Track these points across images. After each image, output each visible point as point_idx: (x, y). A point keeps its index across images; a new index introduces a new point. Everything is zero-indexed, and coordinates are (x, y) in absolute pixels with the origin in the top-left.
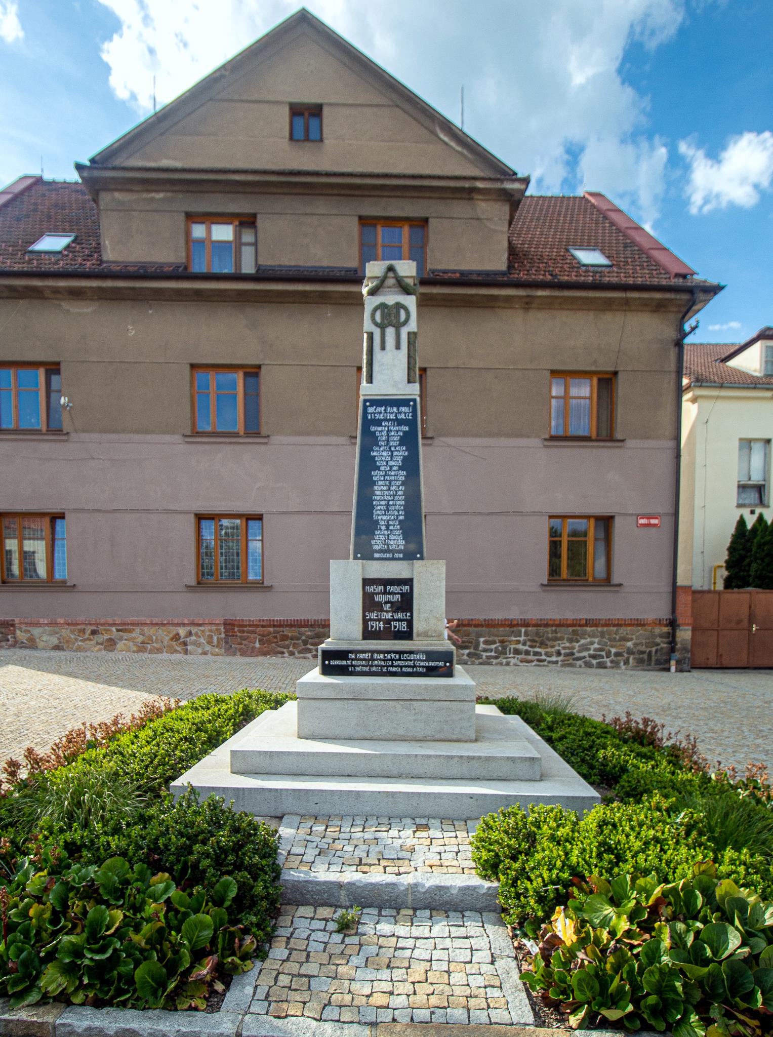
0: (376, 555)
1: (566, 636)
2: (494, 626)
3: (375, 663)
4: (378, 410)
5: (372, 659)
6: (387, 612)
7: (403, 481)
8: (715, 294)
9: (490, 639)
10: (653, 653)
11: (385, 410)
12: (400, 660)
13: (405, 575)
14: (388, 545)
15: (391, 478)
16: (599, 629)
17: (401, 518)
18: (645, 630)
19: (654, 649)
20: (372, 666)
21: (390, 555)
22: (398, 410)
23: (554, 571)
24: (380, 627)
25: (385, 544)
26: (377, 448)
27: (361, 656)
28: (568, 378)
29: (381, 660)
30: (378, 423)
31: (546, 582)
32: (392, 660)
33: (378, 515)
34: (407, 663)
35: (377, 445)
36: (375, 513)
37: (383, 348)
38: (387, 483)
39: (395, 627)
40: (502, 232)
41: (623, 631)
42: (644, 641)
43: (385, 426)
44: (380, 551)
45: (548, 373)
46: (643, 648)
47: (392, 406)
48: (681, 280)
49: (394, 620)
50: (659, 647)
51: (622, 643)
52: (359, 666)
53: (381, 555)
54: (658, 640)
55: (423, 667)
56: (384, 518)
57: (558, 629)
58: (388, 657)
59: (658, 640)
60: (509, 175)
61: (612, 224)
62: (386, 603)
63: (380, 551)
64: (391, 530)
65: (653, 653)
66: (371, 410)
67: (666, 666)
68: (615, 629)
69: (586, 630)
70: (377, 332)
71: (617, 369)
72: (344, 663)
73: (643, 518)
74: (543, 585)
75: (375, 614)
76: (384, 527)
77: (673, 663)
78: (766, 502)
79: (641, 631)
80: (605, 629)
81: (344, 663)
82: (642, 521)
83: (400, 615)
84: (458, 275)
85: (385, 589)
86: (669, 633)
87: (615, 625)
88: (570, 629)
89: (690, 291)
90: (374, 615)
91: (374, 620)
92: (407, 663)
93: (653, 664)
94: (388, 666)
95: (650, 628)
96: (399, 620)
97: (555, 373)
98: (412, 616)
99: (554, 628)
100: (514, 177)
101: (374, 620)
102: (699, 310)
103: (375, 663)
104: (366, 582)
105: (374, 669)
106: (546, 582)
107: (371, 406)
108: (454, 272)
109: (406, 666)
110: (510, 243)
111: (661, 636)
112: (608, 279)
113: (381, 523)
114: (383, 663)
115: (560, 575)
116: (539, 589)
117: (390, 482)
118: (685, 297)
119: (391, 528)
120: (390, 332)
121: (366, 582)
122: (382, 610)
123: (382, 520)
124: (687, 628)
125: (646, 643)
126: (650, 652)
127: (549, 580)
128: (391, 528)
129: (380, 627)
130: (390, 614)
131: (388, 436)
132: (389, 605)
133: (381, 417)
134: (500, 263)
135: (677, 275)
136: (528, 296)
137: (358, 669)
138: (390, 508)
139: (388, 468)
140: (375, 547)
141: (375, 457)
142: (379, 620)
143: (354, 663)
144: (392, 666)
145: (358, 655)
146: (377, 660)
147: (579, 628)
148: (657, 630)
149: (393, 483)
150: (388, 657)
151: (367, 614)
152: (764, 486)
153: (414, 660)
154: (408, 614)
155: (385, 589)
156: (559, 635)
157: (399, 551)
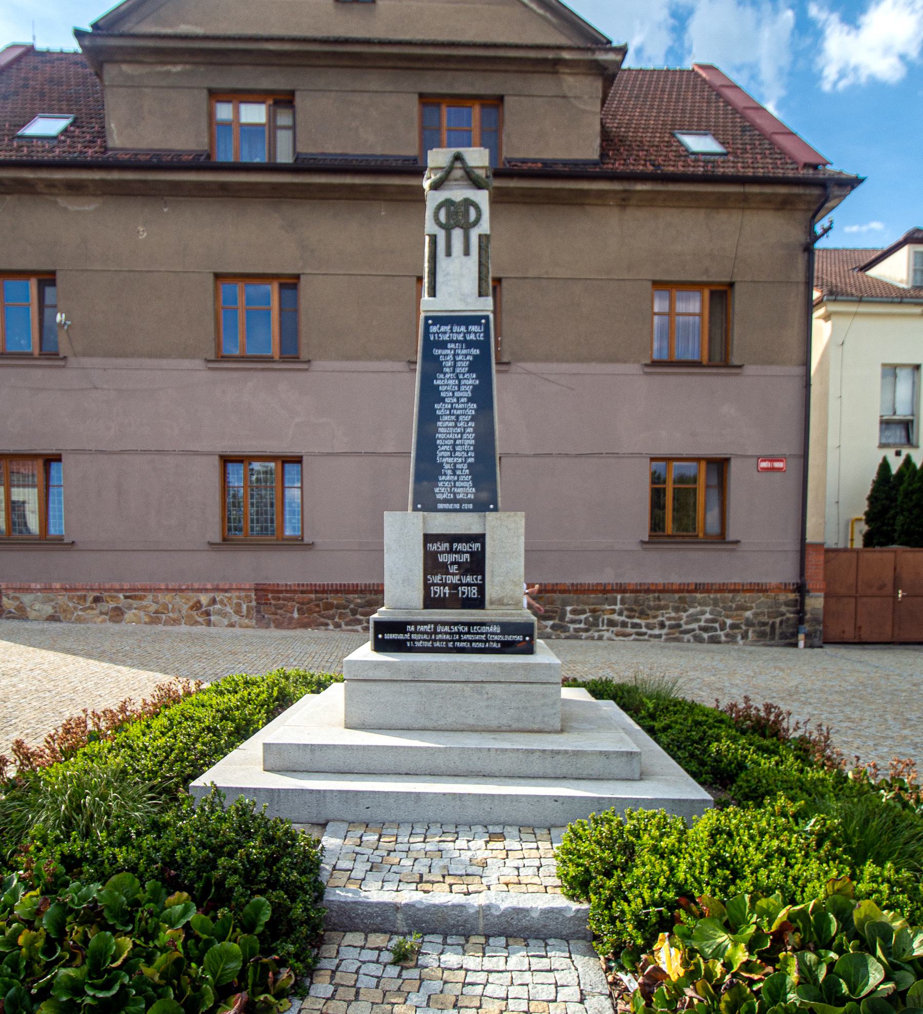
0: (440, 506)
1: (671, 604)
2: (583, 592)
3: (439, 637)
4: (443, 329)
5: (436, 633)
6: (453, 574)
7: (473, 416)
8: (853, 188)
9: (579, 608)
10: (777, 625)
11: (451, 329)
12: (469, 633)
13: (475, 530)
14: (455, 494)
15: (459, 412)
16: (712, 596)
17: (471, 460)
18: (768, 597)
19: (778, 620)
20: (435, 640)
21: (457, 506)
22: (467, 329)
23: (657, 525)
24: (445, 594)
25: (451, 493)
26: (442, 376)
27: (422, 628)
28: (674, 291)
29: (446, 633)
30: (443, 345)
31: (647, 539)
32: (459, 633)
33: (443, 457)
34: (478, 637)
35: (442, 372)
36: (439, 454)
37: (449, 253)
38: (453, 418)
39: (463, 593)
40: (594, 113)
41: (740, 598)
42: (766, 610)
43: (451, 349)
44: (445, 501)
45: (649, 284)
46: (765, 619)
47: (460, 325)
48: (811, 171)
49: (462, 585)
50: (784, 618)
51: (739, 612)
52: (419, 641)
53: (447, 506)
54: (783, 609)
55: (497, 642)
56: (450, 460)
57: (662, 596)
58: (455, 629)
59: (783, 609)
60: (602, 43)
61: (727, 103)
62: (452, 563)
63: (445, 501)
64: (459, 476)
65: (777, 625)
66: (434, 329)
67: (793, 641)
68: (731, 595)
69: (695, 597)
70: (441, 235)
71: (733, 280)
72: (401, 636)
73: (765, 461)
74: (643, 542)
75: (439, 577)
76: (449, 472)
77: (801, 637)
78: (914, 441)
79: (762, 598)
80: (719, 595)
81: (401, 636)
82: (764, 465)
83: (469, 579)
84: (540, 165)
85: (451, 547)
86: (796, 601)
87: (730, 591)
88: (677, 596)
89: (823, 184)
90: (437, 579)
91: (437, 584)
92: (478, 637)
93: (777, 638)
94: (454, 641)
95: (773, 594)
96: (468, 585)
97: (658, 284)
98: (483, 579)
99: (656, 595)
100: (608, 46)
101: (437, 584)
102: (833, 208)
103: (439, 637)
104: (429, 538)
105: (437, 644)
106: (647, 539)
107: (434, 324)
108: (535, 161)
109: (476, 641)
110: (603, 125)
111: (787, 604)
112: (722, 170)
113: (447, 466)
114: (448, 637)
115: (664, 531)
116: (638, 548)
117: (457, 416)
118: (816, 191)
119: (458, 472)
120: (457, 234)
121: (429, 538)
122: (448, 573)
123: (447, 463)
124: (818, 594)
125: (768, 613)
126: (773, 624)
127: (650, 536)
128: (458, 472)
129: (445, 594)
130: (457, 577)
131: (455, 361)
132: (456, 567)
133: (446, 337)
134: (590, 150)
135: (806, 166)
136: (625, 191)
137: (418, 644)
138: (458, 448)
139: (455, 400)
140: (439, 496)
141: (438, 386)
142: (444, 585)
143: (414, 636)
144: (460, 640)
145: (419, 627)
146: (441, 633)
147: (687, 595)
148: (782, 597)
149: (461, 418)
150: (455, 629)
151: (429, 577)
152: (912, 421)
153: (487, 634)
154: (480, 577)
155: (451, 547)
156: (662, 603)
157: (469, 501)
